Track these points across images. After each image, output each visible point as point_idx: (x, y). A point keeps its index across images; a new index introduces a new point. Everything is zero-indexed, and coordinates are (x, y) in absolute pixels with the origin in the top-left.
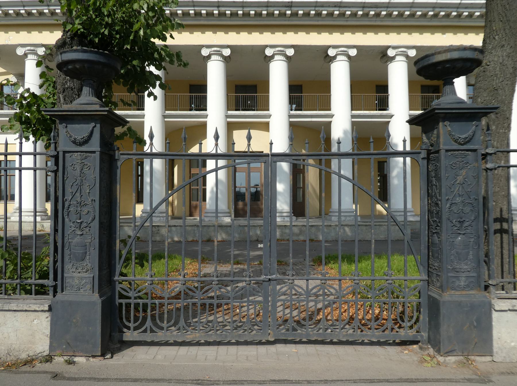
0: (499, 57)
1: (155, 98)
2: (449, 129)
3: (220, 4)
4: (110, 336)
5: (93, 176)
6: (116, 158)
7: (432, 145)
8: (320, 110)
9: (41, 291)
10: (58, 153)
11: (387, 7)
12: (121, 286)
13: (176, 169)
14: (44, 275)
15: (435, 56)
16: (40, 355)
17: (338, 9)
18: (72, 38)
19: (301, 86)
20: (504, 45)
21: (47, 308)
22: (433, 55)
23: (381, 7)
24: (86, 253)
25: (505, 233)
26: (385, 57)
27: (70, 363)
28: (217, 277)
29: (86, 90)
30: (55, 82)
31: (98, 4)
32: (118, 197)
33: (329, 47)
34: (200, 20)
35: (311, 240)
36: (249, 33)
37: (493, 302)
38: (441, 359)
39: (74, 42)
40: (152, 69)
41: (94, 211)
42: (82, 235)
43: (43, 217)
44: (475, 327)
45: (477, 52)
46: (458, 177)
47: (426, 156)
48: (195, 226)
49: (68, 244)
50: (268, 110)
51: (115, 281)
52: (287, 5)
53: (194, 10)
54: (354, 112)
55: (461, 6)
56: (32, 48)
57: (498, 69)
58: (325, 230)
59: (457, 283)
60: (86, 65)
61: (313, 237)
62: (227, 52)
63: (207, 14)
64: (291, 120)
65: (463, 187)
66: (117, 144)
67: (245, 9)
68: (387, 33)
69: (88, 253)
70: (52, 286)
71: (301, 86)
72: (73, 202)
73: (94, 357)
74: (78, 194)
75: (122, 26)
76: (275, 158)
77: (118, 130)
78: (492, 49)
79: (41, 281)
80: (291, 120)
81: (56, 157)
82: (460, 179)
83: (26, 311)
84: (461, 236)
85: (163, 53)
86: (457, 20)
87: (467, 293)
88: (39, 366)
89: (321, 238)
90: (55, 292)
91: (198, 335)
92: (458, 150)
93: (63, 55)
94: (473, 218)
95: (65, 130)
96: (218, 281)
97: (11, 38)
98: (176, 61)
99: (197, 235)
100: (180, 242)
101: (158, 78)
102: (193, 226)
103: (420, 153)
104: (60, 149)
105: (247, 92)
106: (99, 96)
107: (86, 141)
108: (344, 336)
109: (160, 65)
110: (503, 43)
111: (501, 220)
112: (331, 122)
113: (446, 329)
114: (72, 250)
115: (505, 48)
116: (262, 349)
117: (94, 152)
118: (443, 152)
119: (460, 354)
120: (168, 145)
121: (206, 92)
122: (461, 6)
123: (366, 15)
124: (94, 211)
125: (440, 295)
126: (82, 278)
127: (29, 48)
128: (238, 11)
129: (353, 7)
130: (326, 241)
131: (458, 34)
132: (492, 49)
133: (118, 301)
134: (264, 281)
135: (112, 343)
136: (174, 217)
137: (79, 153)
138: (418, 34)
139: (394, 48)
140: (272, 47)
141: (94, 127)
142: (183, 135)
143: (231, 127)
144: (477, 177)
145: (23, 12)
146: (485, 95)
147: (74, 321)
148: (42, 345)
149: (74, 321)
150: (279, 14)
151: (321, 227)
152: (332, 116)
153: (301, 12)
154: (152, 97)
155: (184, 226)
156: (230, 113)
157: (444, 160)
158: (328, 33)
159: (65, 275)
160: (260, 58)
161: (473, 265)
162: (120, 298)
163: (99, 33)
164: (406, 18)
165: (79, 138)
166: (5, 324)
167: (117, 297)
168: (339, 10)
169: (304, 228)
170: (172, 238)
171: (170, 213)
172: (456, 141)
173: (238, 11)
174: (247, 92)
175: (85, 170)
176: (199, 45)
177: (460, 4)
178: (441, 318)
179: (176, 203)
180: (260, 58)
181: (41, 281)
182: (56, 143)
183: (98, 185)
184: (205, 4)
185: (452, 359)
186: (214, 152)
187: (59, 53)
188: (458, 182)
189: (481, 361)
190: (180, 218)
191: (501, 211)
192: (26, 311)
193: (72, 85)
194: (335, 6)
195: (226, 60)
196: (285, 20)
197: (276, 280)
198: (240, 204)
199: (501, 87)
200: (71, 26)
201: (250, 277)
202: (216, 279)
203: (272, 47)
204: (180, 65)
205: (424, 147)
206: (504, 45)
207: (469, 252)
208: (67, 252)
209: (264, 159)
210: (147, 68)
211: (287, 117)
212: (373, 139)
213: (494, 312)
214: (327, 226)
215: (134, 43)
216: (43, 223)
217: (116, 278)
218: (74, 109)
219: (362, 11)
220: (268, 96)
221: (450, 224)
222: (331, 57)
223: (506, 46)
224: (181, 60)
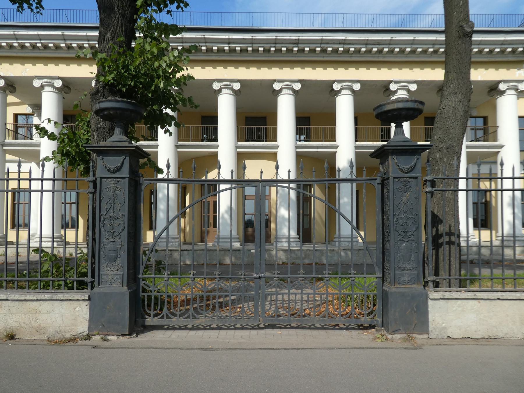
1: (171, 134)
2: (396, 161)
3: (230, 41)
4: (135, 321)
5: (123, 197)
6: (141, 183)
7: (385, 174)
8: (325, 141)
9: (81, 286)
10: (96, 179)
11: (389, 44)
12: (144, 282)
13: (188, 197)
14: (85, 275)
15: (386, 106)
16: (81, 335)
17: (342, 46)
18: (104, 87)
19: (309, 118)
20: (456, 93)
21: (87, 298)
22: (384, 105)
23: (383, 44)
24: (117, 256)
25: (452, 244)
26: (388, 91)
27: (105, 340)
28: (219, 275)
29: (117, 130)
30: (89, 121)
31: (127, 62)
32: (142, 213)
33: (334, 81)
34: (212, 56)
35: (316, 264)
37: (429, 293)
38: (390, 336)
39: (106, 91)
40: (169, 111)
41: (124, 224)
42: (114, 242)
43: (59, 243)
44: (415, 312)
47: (380, 182)
49: (103, 249)
50: (276, 141)
51: (139, 278)
52: (294, 42)
53: (206, 46)
54: (357, 143)
56: (49, 81)
57: (451, 112)
58: (329, 254)
60: (118, 112)
61: (317, 261)
62: (237, 86)
63: (218, 50)
64: (298, 150)
65: (407, 206)
66: (141, 171)
67: (255, 46)
68: (390, 69)
69: (119, 255)
70: (90, 282)
71: (309, 118)
72: (108, 216)
73: (123, 335)
74: (111, 210)
75: (145, 79)
76: (264, 183)
77: (142, 161)
78: (447, 96)
79: (81, 279)
80: (298, 150)
81: (94, 183)
82: (404, 199)
83: (70, 300)
85: (177, 99)
87: (410, 286)
88: (80, 342)
89: (325, 262)
90: (92, 288)
91: (204, 320)
92: (403, 177)
93: (101, 104)
94: (414, 229)
95: (102, 161)
96: (220, 278)
97: (27, 70)
98: (188, 104)
100: (190, 265)
101: (172, 118)
103: (376, 179)
104: (98, 174)
105: (256, 124)
106: (126, 134)
107: (118, 170)
109: (175, 107)
110: (456, 90)
111: (450, 234)
112: (336, 152)
113: (393, 313)
114: (107, 254)
116: (254, 332)
117: (124, 178)
118: (391, 179)
119: (404, 332)
120: (181, 173)
121: (217, 123)
124: (124, 224)
125: (389, 288)
126: (114, 275)
127: (46, 80)
128: (247, 47)
130: (329, 265)
132: (447, 96)
133: (141, 294)
134: (255, 278)
135: (137, 326)
136: (185, 243)
137: (112, 179)
138: (419, 69)
139: (396, 82)
140: (280, 81)
141: (124, 159)
142: (193, 166)
143: (241, 158)
144: (417, 198)
145: (39, 45)
147: (108, 307)
148: (83, 328)
149: (108, 307)
150: (286, 51)
151: (324, 251)
152: (337, 147)
153: (307, 49)
154: (168, 134)
155: (194, 251)
156: (240, 143)
157: (392, 185)
158: (333, 69)
159: (101, 273)
160: (268, 92)
161: (415, 265)
162: (143, 292)
163: (127, 85)
164: (407, 54)
165: (113, 167)
166: (53, 311)
167: (141, 291)
168: (343, 47)
169: (309, 252)
170: (184, 262)
171: (182, 239)
172: (401, 171)
173: (247, 47)
174: (256, 124)
175: (117, 192)
178: (389, 305)
179: (188, 229)
180: (268, 92)
181: (81, 279)
182: (94, 171)
183: (127, 203)
184: (215, 41)
185: (398, 336)
186: (217, 178)
187: (97, 102)
188: (403, 201)
189: (419, 338)
190: (190, 244)
192: (70, 300)
193: (104, 125)
194: (340, 43)
195: (236, 93)
196: (292, 56)
197: (265, 277)
198: (250, 230)
200: (103, 78)
201: (244, 275)
202: (218, 277)
203: (280, 81)
204: (192, 107)
205: (379, 175)
207: (411, 255)
208: (102, 255)
209: (256, 183)
210: (164, 110)
211: (294, 148)
212: (366, 168)
213: (429, 300)
214: (330, 250)
215: (154, 92)
216: (59, 249)
217: (140, 276)
218: (109, 145)
219: (366, 47)
220: (276, 128)
221: (396, 234)
222: (336, 91)
224: (192, 103)
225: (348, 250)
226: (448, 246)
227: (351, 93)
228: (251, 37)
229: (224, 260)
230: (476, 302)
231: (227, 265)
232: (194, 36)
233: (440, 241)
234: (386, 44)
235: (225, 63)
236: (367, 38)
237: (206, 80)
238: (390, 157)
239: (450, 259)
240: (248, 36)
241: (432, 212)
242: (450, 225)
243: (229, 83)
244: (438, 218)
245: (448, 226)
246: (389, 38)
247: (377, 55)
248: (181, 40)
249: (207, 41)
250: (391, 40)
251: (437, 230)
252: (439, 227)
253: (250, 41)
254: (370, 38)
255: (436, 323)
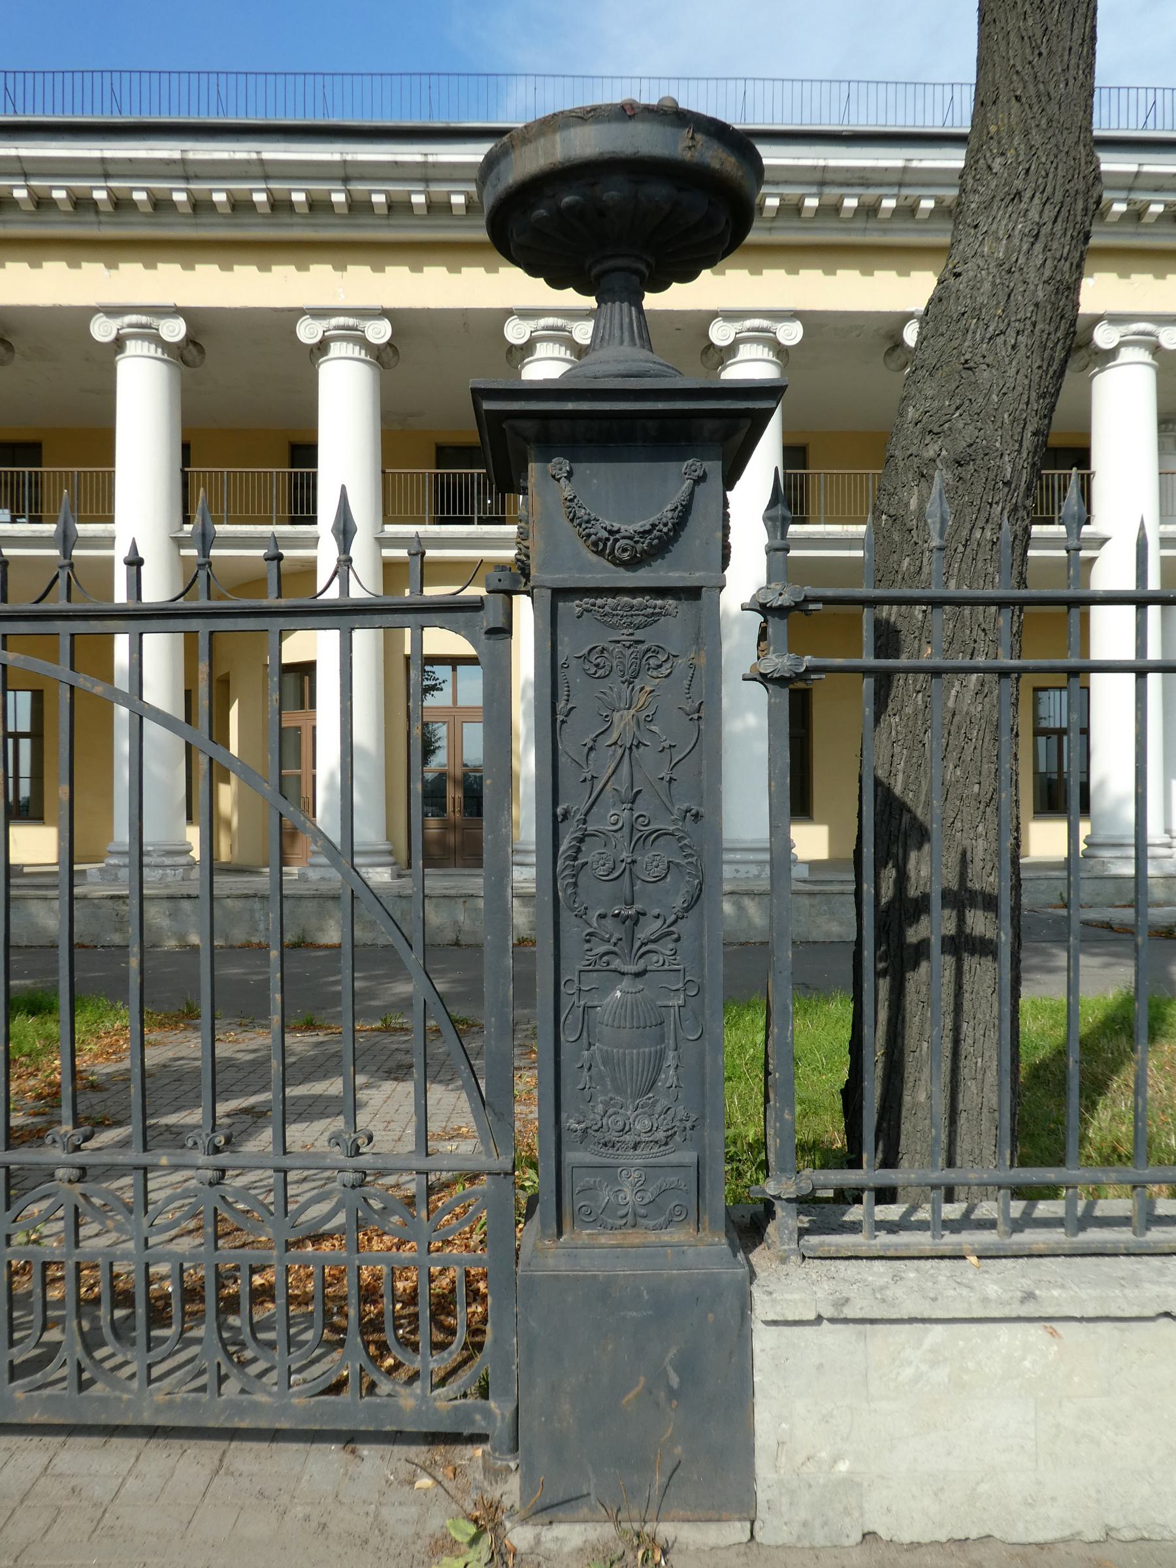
0: (999, 240)
3: (351, 171)
11: (900, 185)
20: (1019, 194)
23: (880, 185)
26: (899, 350)
33: (714, 315)
34: (291, 225)
36: (450, 271)
44: (672, 1394)
45: (686, 133)
46: (616, 716)
48: (255, 896)
53: (269, 191)
55: (1140, 182)
57: (987, 286)
59: (605, 1196)
62: (380, 332)
84: (626, 982)
86: (1130, 229)
87: (652, 1237)
94: (679, 902)
99: (262, 926)
102: (247, 897)
108: (158, 1410)
110: (1018, 184)
115: (1023, 206)
122: (1140, 182)
123: (831, 210)
129: (787, 183)
131: (1135, 277)
146: (930, 393)
156: (392, 529)
170: (182, 937)
176: (290, 310)
177: (1137, 174)
191: (964, 861)
195: (381, 357)
199: (989, 360)
206: (1019, 194)
219: (820, 195)
223: (1027, 195)
225: (750, 894)
226: (949, 960)
227: (770, 356)
228: (419, 158)
229: (321, 929)
230: (1035, 1331)
231: (327, 947)
232: (225, 156)
233: (913, 935)
234: (890, 185)
235: (340, 251)
236: (821, 163)
237: (275, 310)
238: (533, 468)
239: (956, 1029)
240: (410, 153)
241: (877, 783)
242: (964, 854)
243: (351, 321)
244: (906, 818)
245: (953, 859)
246: (900, 163)
247: (860, 224)
248: (179, 170)
249: (271, 170)
250: (905, 169)
251: (902, 879)
252: (911, 865)
253: (419, 173)
254: (832, 163)
255: (800, 1458)
